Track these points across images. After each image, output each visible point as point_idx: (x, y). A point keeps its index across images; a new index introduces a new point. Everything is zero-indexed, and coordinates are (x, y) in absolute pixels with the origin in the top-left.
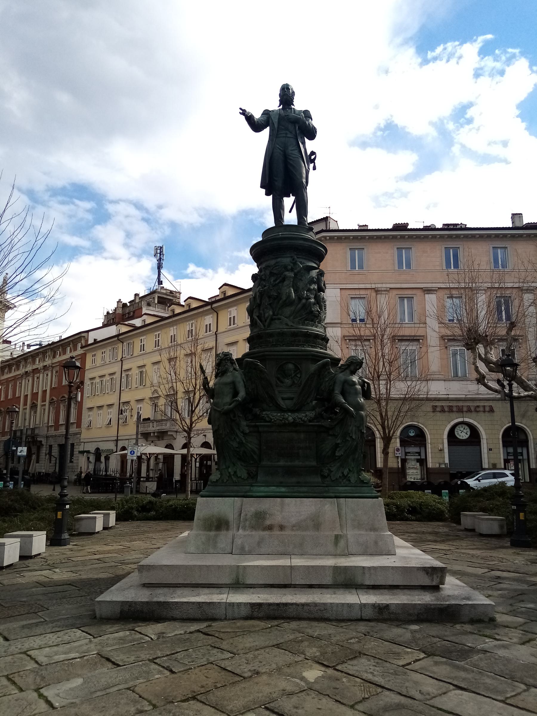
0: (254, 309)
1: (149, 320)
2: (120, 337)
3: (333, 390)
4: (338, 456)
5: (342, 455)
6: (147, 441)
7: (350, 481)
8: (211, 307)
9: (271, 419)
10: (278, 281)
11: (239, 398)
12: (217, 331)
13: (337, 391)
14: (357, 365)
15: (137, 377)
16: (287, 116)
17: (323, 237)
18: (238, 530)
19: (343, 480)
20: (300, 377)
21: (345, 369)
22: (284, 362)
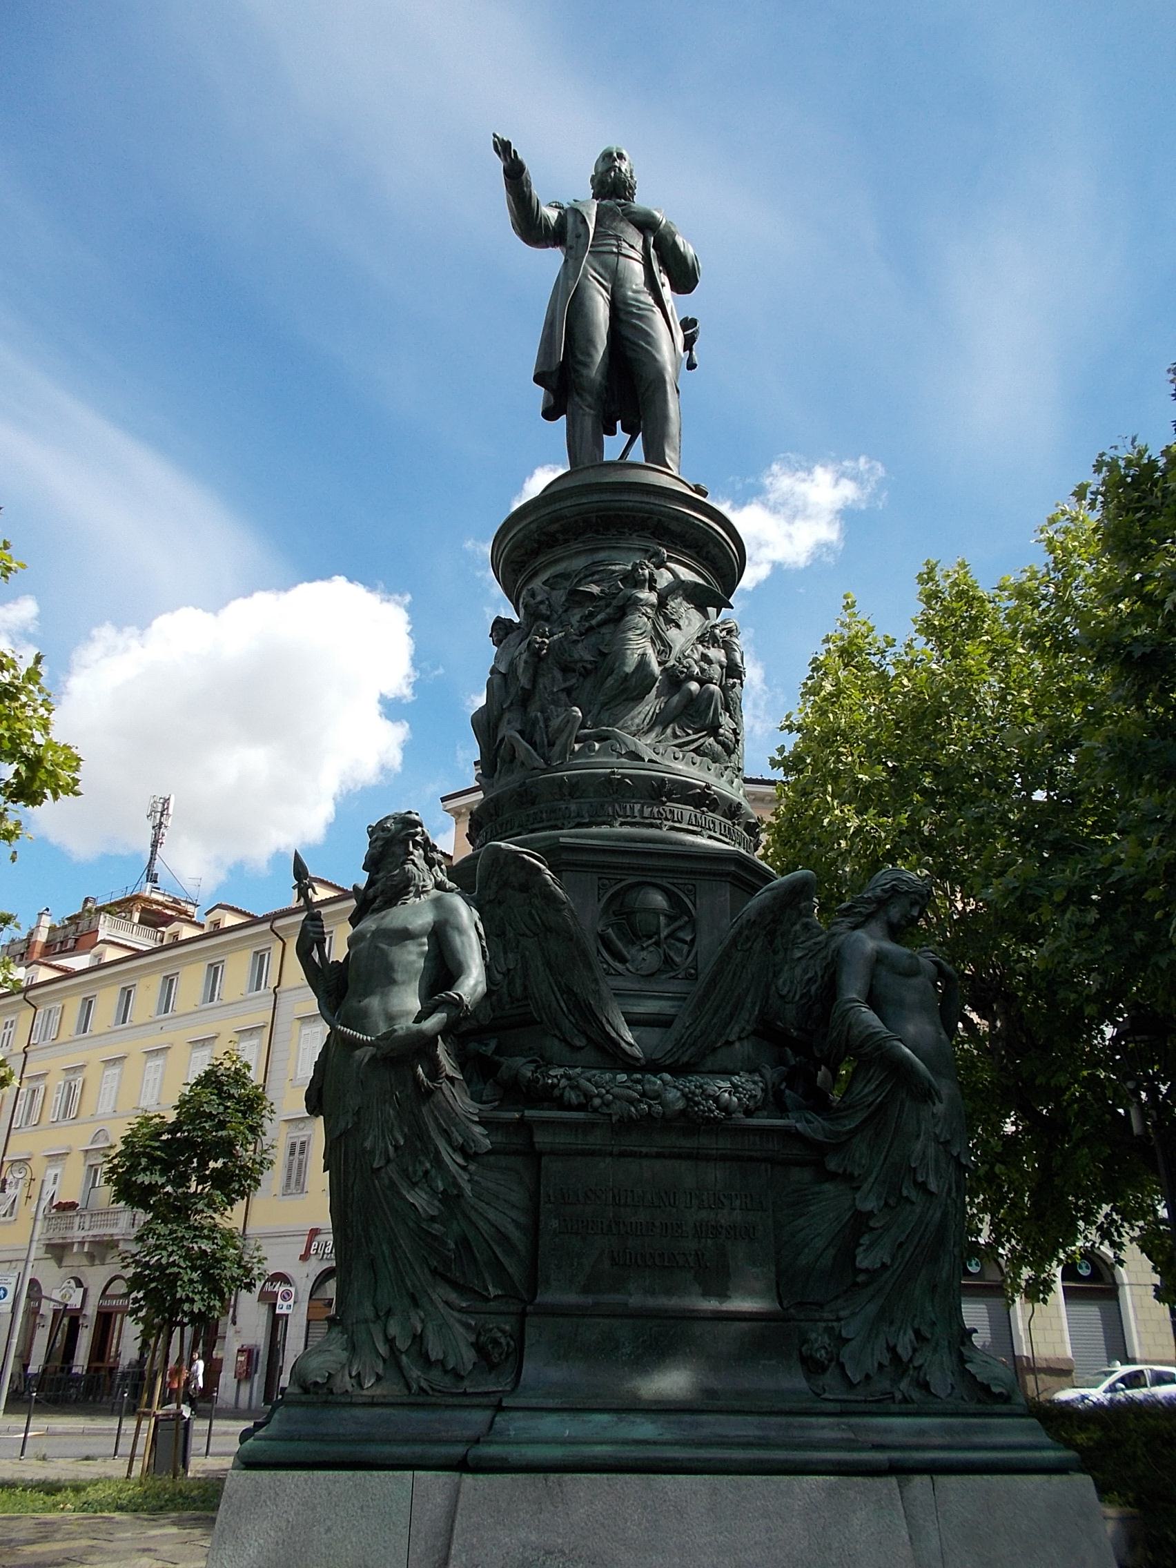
1: (111, 954)
2: (31, 994)
4: (866, 1271)
5: (884, 1265)
6: (60, 1267)
7: (925, 1386)
8: (271, 927)
9: (588, 1097)
12: (278, 986)
13: (853, 989)
14: (913, 904)
15: (60, 1095)
20: (693, 940)
21: (870, 917)
22: (631, 880)
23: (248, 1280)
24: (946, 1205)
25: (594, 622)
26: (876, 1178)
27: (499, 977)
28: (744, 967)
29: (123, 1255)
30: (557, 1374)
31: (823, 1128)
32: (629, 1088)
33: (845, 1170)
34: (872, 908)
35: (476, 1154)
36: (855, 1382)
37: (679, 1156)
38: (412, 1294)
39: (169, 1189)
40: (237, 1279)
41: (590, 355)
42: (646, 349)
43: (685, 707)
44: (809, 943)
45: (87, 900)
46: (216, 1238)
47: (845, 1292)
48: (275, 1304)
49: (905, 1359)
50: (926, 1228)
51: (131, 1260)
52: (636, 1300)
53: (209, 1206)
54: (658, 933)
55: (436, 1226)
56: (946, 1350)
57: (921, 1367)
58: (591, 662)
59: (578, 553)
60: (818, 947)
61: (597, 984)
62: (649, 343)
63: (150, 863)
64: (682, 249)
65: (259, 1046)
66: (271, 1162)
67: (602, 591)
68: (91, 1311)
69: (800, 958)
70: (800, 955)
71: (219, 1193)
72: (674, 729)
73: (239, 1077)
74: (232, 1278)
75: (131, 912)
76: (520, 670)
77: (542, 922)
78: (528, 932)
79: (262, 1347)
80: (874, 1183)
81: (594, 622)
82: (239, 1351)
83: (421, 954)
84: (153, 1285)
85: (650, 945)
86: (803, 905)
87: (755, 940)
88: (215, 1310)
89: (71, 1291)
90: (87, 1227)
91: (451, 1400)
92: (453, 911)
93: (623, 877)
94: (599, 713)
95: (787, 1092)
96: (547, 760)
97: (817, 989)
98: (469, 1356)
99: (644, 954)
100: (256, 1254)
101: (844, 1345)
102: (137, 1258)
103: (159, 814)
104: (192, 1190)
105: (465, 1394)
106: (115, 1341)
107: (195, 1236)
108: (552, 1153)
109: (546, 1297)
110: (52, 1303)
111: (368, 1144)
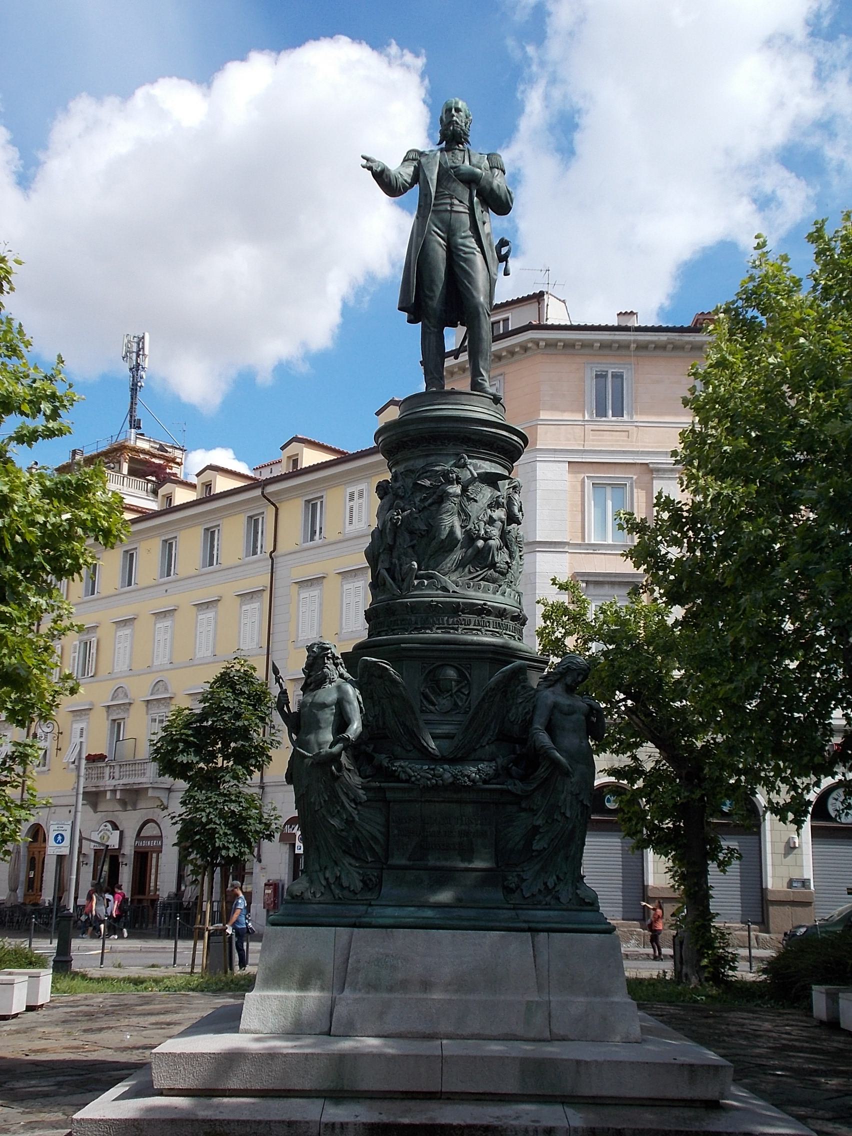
0: (379, 554)
3: (531, 722)
6: (96, 812)
7: (558, 899)
8: (263, 493)
9: (410, 776)
10: (430, 501)
12: (274, 551)
13: (538, 725)
14: (579, 675)
15: (77, 654)
16: (456, 167)
17: (532, 340)
18: (343, 991)
19: (545, 897)
20: (469, 694)
21: (556, 681)
23: (268, 833)
25: (426, 504)
27: (371, 719)
29: (173, 815)
32: (428, 773)
34: (556, 677)
35: (360, 802)
37: (452, 802)
39: (202, 765)
40: (260, 832)
41: (433, 291)
42: (468, 288)
43: (475, 555)
44: (525, 695)
45: (74, 453)
46: (241, 802)
48: (294, 844)
51: (179, 818)
52: (432, 863)
53: (234, 778)
54: (451, 690)
58: (424, 530)
59: (419, 457)
62: (474, 272)
63: (131, 408)
64: (497, 192)
65: (261, 610)
66: (279, 742)
67: (431, 484)
68: (128, 850)
70: (520, 701)
71: (240, 767)
72: (469, 569)
73: (247, 678)
74: (256, 831)
75: (119, 462)
76: (388, 530)
79: (286, 882)
82: (266, 885)
83: (332, 714)
84: (198, 837)
88: (245, 854)
89: (109, 833)
90: (117, 776)
91: (353, 902)
92: (346, 693)
98: (360, 885)
99: (444, 701)
100: (272, 813)
102: (183, 817)
103: (134, 355)
104: (220, 765)
105: (357, 900)
106: (153, 877)
107: (225, 801)
109: (392, 861)
110: (93, 844)
111: (312, 800)
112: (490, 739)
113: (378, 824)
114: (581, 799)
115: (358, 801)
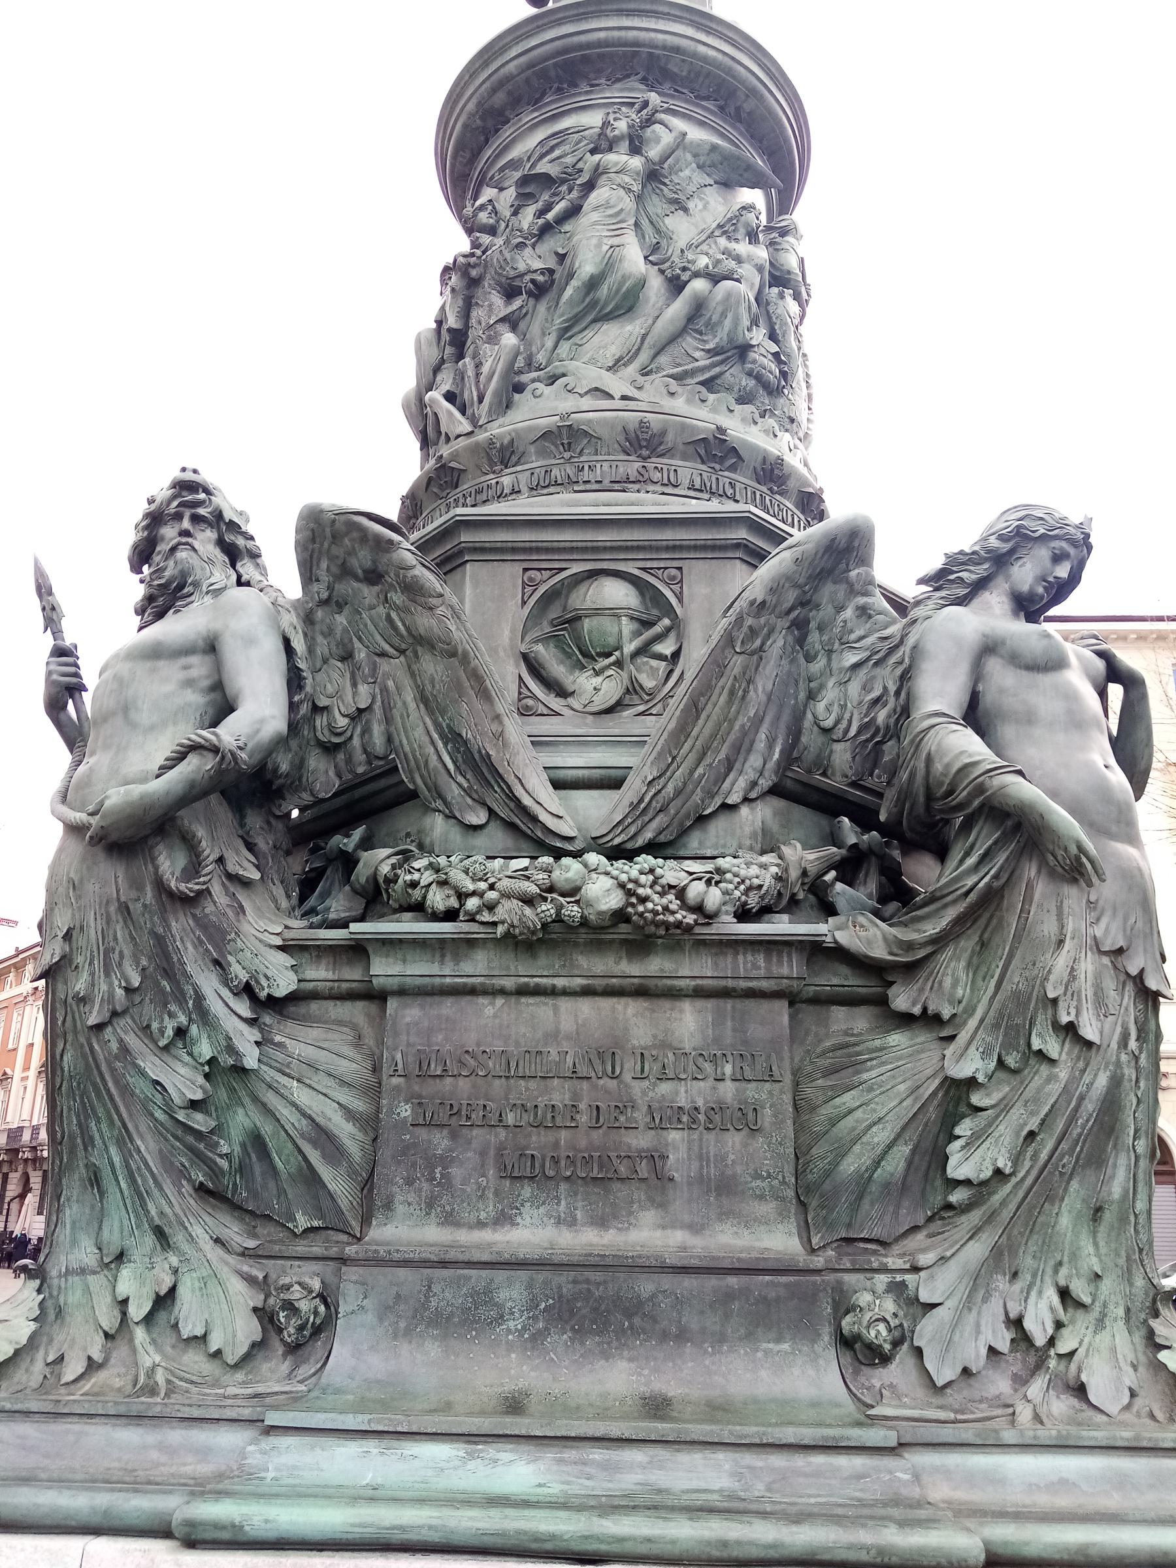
4: (967, 1182)
5: (998, 1172)
7: (1080, 1390)
9: (462, 896)
11: (230, 733)
14: (1057, 558)
20: (676, 655)
21: (980, 585)
22: (576, 568)
24: (1118, 1064)
25: (550, 216)
26: (982, 1021)
28: (749, 682)
30: (377, 1364)
31: (885, 939)
33: (925, 1009)
34: (982, 570)
36: (940, 1383)
38: (158, 1227)
47: (930, 1219)
49: (1040, 1341)
50: (1078, 1106)
54: (619, 648)
55: (199, 1116)
56: (1121, 1324)
57: (1072, 1354)
58: (542, 272)
60: (887, 645)
61: (501, 723)
69: (856, 666)
77: (407, 629)
78: (387, 647)
80: (978, 1028)
81: (550, 216)
85: (608, 667)
86: (853, 574)
87: (768, 636)
93: (563, 565)
94: (556, 347)
95: (839, 886)
96: (474, 421)
97: (889, 716)
101: (924, 1315)
108: (402, 992)
112: (754, 784)
113: (343, 1083)
114: (1134, 971)
115: (263, 995)
